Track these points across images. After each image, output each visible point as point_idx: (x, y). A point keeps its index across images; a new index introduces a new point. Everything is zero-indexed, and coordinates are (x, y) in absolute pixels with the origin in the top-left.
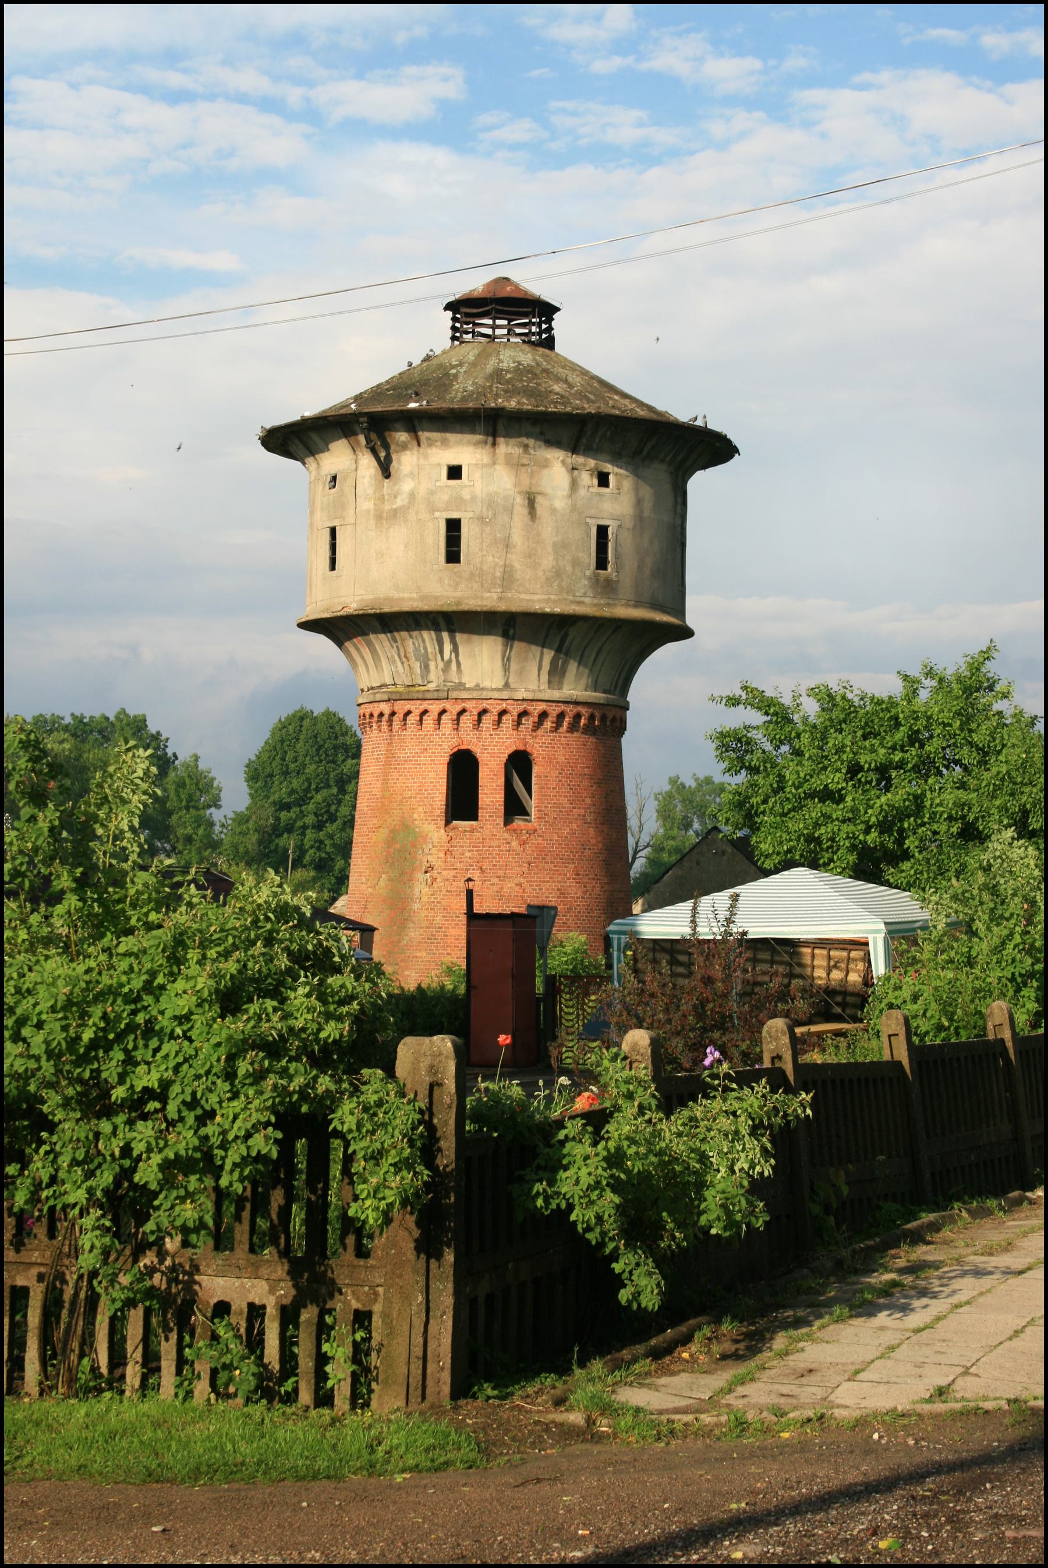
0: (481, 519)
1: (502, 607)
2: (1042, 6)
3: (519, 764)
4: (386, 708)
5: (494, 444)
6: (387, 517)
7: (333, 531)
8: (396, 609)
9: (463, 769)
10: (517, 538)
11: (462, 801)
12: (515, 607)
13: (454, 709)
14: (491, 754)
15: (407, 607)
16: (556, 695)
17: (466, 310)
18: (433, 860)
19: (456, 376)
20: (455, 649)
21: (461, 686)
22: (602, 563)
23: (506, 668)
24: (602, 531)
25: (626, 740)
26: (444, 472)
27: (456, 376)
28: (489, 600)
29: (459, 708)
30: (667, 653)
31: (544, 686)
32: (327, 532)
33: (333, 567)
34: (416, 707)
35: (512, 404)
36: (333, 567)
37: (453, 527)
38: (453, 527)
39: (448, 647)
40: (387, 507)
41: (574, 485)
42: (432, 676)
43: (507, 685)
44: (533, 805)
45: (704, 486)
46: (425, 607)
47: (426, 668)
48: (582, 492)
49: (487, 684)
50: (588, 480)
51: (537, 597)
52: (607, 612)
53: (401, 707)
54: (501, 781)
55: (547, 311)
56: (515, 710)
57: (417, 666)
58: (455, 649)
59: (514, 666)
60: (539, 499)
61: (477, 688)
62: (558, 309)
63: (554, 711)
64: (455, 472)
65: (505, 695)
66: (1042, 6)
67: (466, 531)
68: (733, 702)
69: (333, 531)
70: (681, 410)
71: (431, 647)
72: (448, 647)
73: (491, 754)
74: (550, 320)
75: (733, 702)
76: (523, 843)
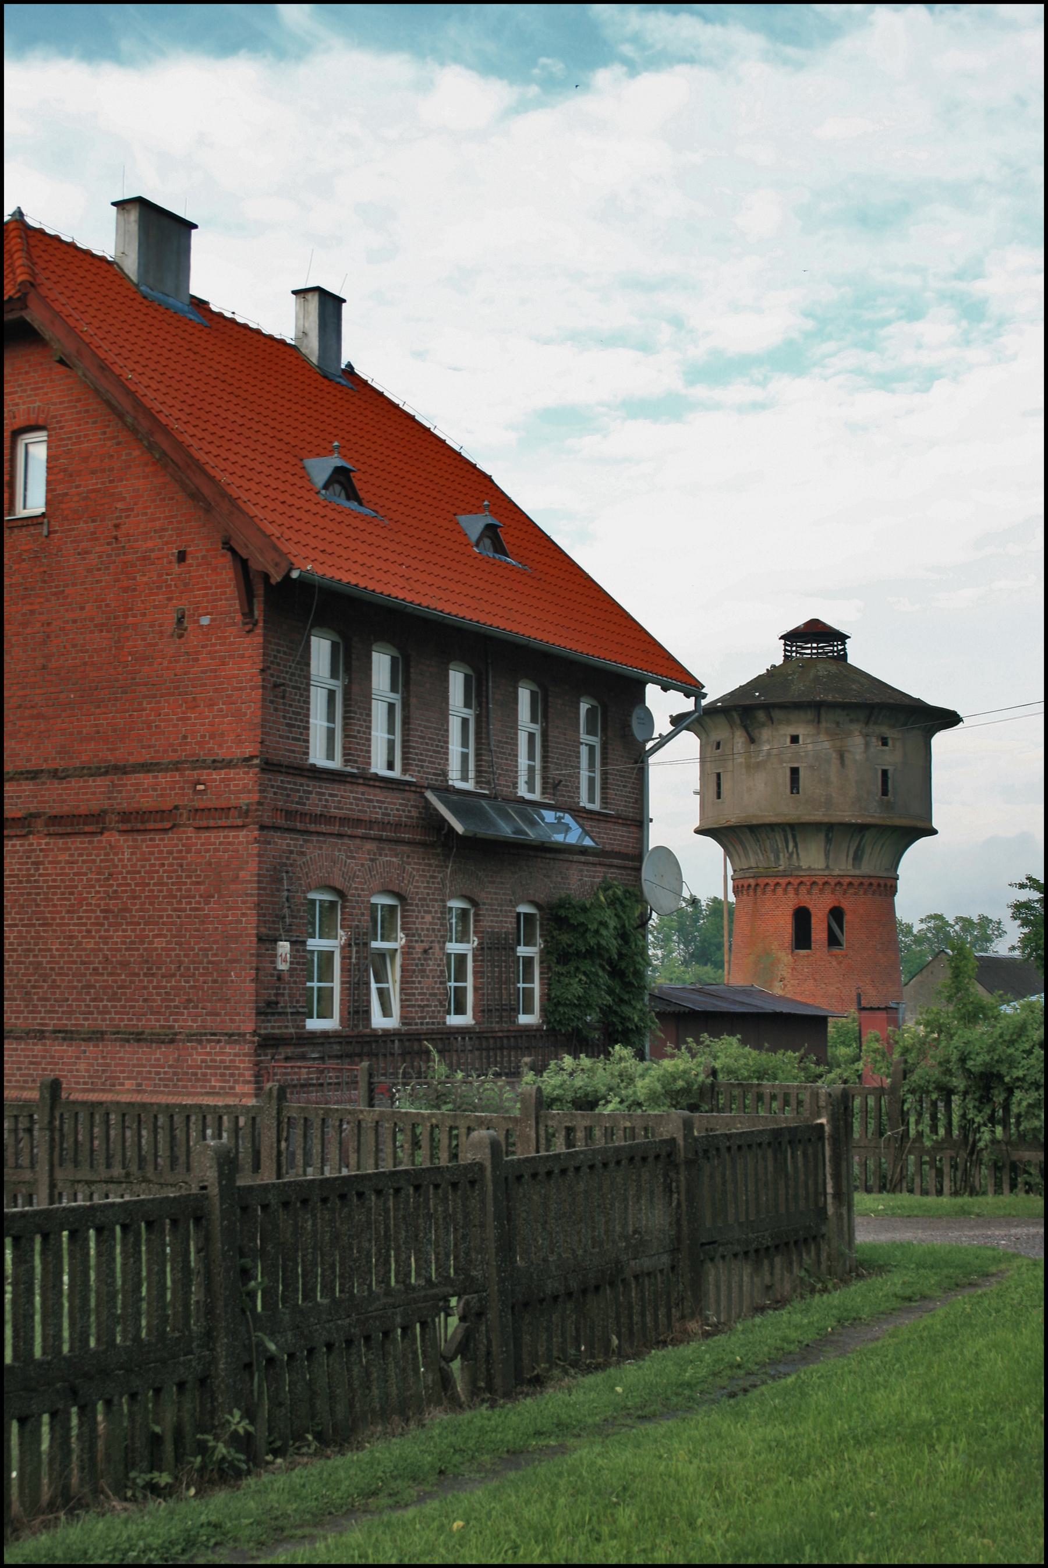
0: (811, 767)
1: (826, 820)
2: (1042, 6)
3: (837, 914)
4: (752, 882)
5: (819, 722)
6: (752, 767)
7: (718, 775)
8: (761, 822)
9: (802, 918)
10: (834, 779)
11: (802, 938)
12: (834, 820)
13: (796, 882)
14: (819, 908)
15: (767, 820)
16: (857, 872)
17: (791, 638)
18: (784, 973)
19: (792, 681)
20: (796, 846)
21: (799, 868)
22: (885, 793)
23: (827, 856)
24: (885, 773)
25: (897, 898)
26: (788, 740)
27: (792, 681)
28: (818, 816)
29: (798, 881)
30: (922, 844)
31: (850, 867)
32: (715, 777)
33: (719, 797)
34: (772, 881)
35: (830, 698)
36: (719, 797)
37: (795, 771)
38: (795, 771)
39: (791, 845)
40: (753, 760)
41: (867, 745)
42: (782, 862)
43: (827, 867)
44: (844, 939)
45: (942, 741)
46: (778, 820)
47: (777, 858)
48: (872, 750)
49: (816, 866)
50: (874, 741)
51: (849, 815)
52: (888, 822)
53: (762, 881)
54: (825, 926)
55: (842, 638)
56: (833, 882)
57: (772, 857)
58: (796, 846)
59: (831, 855)
60: (847, 755)
61: (809, 869)
62: (344, 301)
63: (856, 882)
64: (795, 739)
65: (826, 873)
66: (1042, 6)
67: (802, 773)
68: (1022, 886)
69: (718, 775)
70: (934, 699)
71: (781, 845)
72: (791, 845)
73: (819, 908)
74: (844, 644)
75: (1022, 886)
76: (839, 963)
